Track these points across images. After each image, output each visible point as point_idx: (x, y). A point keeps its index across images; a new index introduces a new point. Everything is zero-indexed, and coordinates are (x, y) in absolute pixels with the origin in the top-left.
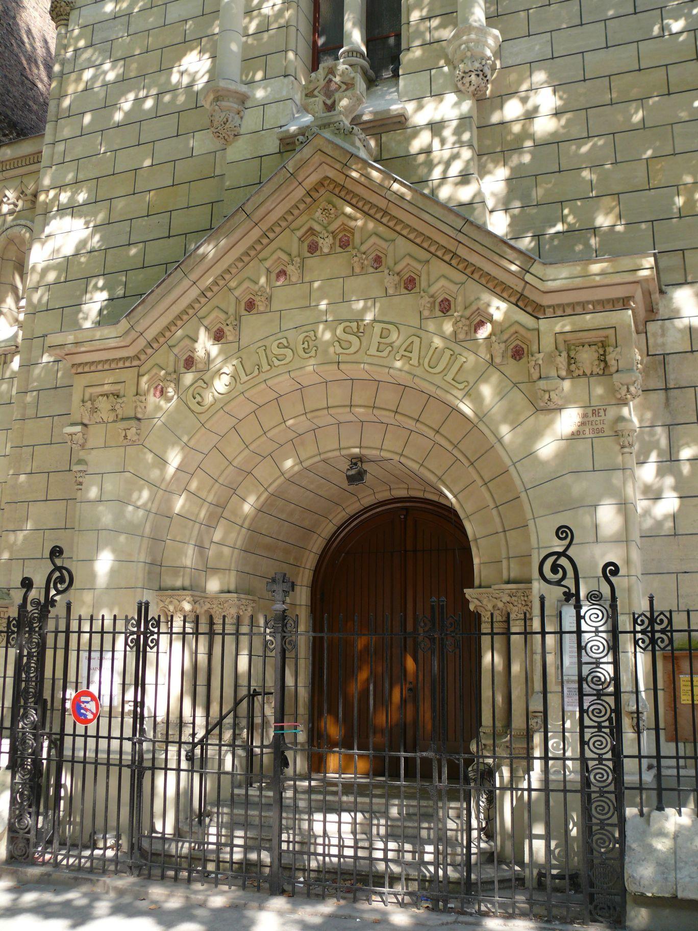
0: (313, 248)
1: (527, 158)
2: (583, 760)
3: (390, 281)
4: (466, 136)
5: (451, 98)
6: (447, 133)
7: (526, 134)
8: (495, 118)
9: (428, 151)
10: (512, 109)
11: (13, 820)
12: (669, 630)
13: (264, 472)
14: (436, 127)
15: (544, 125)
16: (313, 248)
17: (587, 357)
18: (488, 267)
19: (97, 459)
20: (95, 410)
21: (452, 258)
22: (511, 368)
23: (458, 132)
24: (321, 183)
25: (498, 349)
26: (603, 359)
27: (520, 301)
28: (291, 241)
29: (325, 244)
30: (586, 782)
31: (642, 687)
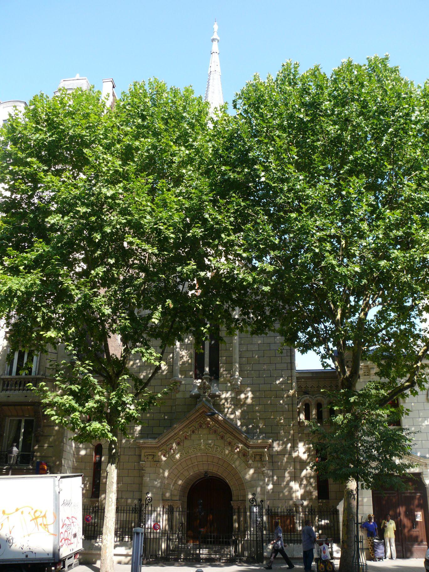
0: (201, 426)
1: (245, 408)
2: (257, 535)
3: (218, 437)
4: (232, 403)
5: (229, 393)
6: (229, 401)
7: (245, 403)
8: (238, 397)
9: (224, 404)
10: (243, 396)
11: (222, 564)
12: (271, 512)
13: (186, 474)
14: (226, 399)
15: (249, 401)
16: (201, 426)
17: (258, 458)
18: (237, 435)
19: (148, 470)
20: (148, 458)
21: (232, 434)
22: (243, 458)
23: (231, 401)
24: (203, 412)
25: (241, 454)
26: (261, 458)
27: (245, 444)
28: (197, 425)
29: (204, 427)
30: (257, 540)
31: (185, 424)
